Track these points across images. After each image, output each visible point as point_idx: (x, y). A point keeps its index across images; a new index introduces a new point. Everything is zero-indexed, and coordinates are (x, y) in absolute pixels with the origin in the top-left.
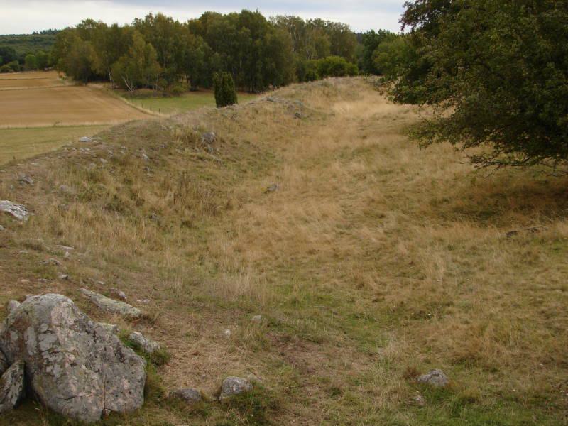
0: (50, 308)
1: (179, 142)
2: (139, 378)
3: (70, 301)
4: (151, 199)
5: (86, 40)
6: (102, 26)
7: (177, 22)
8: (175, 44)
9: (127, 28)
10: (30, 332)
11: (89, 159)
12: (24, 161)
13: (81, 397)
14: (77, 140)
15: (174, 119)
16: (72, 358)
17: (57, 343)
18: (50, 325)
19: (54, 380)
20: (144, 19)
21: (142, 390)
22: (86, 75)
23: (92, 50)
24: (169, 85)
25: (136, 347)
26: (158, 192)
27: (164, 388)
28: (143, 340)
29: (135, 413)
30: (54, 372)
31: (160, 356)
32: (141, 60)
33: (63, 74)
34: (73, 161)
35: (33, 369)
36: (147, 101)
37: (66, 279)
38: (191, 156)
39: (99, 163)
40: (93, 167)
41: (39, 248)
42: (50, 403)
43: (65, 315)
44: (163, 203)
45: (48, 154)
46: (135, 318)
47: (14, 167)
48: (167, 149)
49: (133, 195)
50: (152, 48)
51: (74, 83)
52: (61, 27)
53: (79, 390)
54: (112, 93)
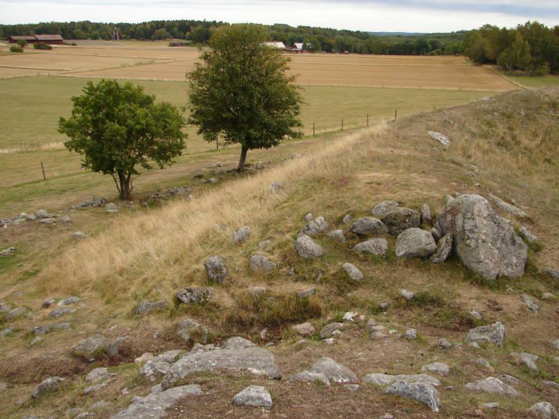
0: (474, 204)
1: (546, 106)
2: (523, 257)
3: (486, 201)
4: (525, 142)
5: (485, 37)
6: (496, 29)
7: (504, 29)
8: (543, 42)
9: (512, 30)
10: (459, 217)
11: (487, 112)
12: (448, 109)
13: (486, 263)
14: (480, 99)
15: (543, 90)
16: (484, 237)
17: (476, 226)
18: (473, 214)
20: (524, 25)
21: (524, 265)
22: (482, 59)
23: (488, 43)
24: (535, 69)
25: (523, 236)
26: (530, 138)
27: (538, 267)
28: (527, 233)
29: (517, 279)
31: (537, 245)
32: (519, 52)
33: (468, 58)
34: (478, 112)
35: (458, 238)
36: (519, 78)
37: (479, 186)
39: (493, 115)
40: (489, 117)
41: (459, 164)
42: (465, 263)
43: (482, 210)
44: (533, 145)
45: (462, 107)
46: (522, 218)
47: (441, 113)
48: (538, 110)
49: (514, 138)
50: (527, 44)
52: (469, 29)
53: (485, 259)
54: (497, 71)
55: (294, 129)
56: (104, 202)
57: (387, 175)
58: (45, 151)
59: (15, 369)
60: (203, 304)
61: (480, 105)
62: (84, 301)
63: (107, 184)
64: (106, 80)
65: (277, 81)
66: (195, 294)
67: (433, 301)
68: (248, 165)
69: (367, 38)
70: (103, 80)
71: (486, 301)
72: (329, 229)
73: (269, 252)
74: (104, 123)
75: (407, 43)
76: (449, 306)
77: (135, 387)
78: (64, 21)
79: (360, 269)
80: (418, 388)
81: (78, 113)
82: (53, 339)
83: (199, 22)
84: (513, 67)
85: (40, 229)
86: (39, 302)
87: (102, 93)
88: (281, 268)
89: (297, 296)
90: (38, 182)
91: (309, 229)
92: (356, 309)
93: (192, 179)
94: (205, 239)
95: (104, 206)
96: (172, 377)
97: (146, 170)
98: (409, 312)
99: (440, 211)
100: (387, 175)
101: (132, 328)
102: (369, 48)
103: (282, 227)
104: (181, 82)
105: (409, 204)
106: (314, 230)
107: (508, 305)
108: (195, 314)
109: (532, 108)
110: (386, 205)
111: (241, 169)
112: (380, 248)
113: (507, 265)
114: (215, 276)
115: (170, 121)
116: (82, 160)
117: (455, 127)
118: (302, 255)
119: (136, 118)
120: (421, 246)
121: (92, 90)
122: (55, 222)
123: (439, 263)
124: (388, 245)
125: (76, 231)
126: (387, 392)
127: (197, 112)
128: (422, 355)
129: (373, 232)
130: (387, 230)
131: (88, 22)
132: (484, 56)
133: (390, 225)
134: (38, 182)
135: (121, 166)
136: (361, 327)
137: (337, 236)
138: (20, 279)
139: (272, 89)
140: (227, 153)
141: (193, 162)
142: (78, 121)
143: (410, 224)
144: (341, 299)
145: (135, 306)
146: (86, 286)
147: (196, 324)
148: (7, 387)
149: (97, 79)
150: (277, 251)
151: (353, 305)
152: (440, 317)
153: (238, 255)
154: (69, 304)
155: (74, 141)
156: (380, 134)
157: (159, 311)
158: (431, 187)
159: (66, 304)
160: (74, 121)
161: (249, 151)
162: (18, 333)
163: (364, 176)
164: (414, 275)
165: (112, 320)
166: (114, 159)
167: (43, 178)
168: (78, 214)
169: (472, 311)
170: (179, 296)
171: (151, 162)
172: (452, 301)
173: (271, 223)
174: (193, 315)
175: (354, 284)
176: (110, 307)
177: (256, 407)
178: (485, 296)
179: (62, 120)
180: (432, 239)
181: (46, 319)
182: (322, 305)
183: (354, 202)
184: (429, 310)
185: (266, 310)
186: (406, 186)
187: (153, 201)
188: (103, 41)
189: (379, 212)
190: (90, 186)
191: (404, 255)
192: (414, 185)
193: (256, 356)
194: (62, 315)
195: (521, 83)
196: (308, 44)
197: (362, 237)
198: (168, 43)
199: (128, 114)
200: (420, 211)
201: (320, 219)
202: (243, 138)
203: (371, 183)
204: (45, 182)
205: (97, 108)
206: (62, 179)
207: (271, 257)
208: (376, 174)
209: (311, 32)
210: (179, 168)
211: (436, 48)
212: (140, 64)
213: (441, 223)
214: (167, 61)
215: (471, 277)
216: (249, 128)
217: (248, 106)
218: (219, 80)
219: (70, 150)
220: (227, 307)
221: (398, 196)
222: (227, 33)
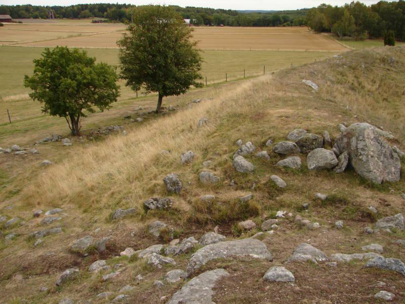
0: (364, 129)
1: (378, 61)
4: (368, 86)
5: (322, 13)
6: (329, 7)
7: (336, 7)
8: (363, 16)
10: (354, 140)
11: (338, 66)
12: (311, 64)
16: (372, 153)
17: (366, 146)
18: (364, 137)
19: (363, 162)
21: (399, 173)
22: (320, 29)
23: (324, 17)
28: (398, 150)
29: (396, 183)
30: (363, 159)
33: (310, 28)
34: (333, 66)
36: (348, 42)
38: (384, 68)
40: (341, 69)
42: (359, 172)
46: (391, 140)
48: (373, 64)
49: (360, 84)
51: (314, 32)
54: (332, 37)
55: (198, 81)
56: (60, 138)
57: (291, 111)
58: (7, 102)
59: (27, 264)
60: (167, 210)
61: (333, 60)
62: (66, 211)
63: (62, 124)
64: (60, 47)
65: (184, 46)
66: (160, 202)
67: (340, 201)
68: (163, 108)
69: (236, 15)
70: (58, 47)
71: (378, 199)
72: (256, 150)
73: (211, 169)
74: (59, 78)
75: (265, 18)
76: (353, 204)
77: (147, 273)
78: (11, 5)
79: (284, 180)
80: (393, 262)
81: (39, 72)
82: (51, 241)
83: (113, 5)
84: (343, 34)
85: (15, 159)
86: (28, 214)
87: (57, 57)
88: (224, 180)
89: (240, 201)
90: (5, 124)
91: (242, 151)
92: (284, 209)
93: (122, 119)
94: (156, 161)
95: (61, 141)
96: (196, 264)
97: (90, 113)
98: (324, 209)
99: (337, 136)
100: (290, 111)
101: (112, 230)
102: (238, 23)
103: (219, 151)
104: (103, 49)
105: (313, 131)
106: (245, 152)
107: (393, 202)
108: (161, 217)
109: (370, 62)
110: (298, 132)
111: (159, 111)
112: (296, 164)
113: (388, 173)
114: (172, 188)
115: (108, 76)
116: (42, 107)
117: (319, 77)
118: (239, 170)
119: (83, 74)
120: (328, 161)
121: (48, 54)
122: (26, 154)
123: (340, 173)
124: (301, 161)
125: (43, 160)
126: (368, 266)
127: (125, 70)
128: (355, 239)
129: (290, 152)
130: (300, 150)
131: (30, 5)
132: (322, 26)
133: (302, 146)
134: (5, 124)
135: (73, 110)
136: (291, 222)
137: (263, 156)
138: (7, 197)
139: (182, 51)
140: (147, 99)
141: (120, 107)
142: (38, 78)
143: (316, 145)
144: (271, 202)
145: (111, 214)
146: (64, 200)
147: (163, 225)
148: (23, 278)
149: (52, 47)
150: (219, 168)
151: (282, 206)
152: (347, 212)
153: (187, 172)
154: (55, 213)
155: (37, 93)
156: (269, 82)
157: (131, 216)
158: (325, 118)
159: (52, 214)
160: (37, 78)
161: (164, 98)
162: (20, 237)
163: (275, 112)
164: (323, 183)
165: (95, 224)
166: (68, 105)
167: (9, 121)
168: (43, 147)
169: (370, 207)
170: (146, 204)
171: (95, 108)
172: (354, 201)
173: (209, 148)
174: (160, 218)
175: (281, 191)
176: (89, 215)
177: (285, 282)
178: (376, 196)
179: (27, 77)
180: (334, 156)
181: (39, 226)
182: (259, 207)
183: (272, 131)
184: (337, 207)
185: (217, 212)
186: (307, 118)
187: (97, 136)
188: (42, 20)
189: (293, 138)
190: (46, 127)
191: (314, 168)
192: (313, 118)
193: (253, 244)
194: (51, 222)
195: (350, 46)
196: (194, 20)
197: (282, 156)
198: (91, 21)
199: (77, 72)
200: (323, 136)
201: (249, 144)
202: (161, 88)
203: (281, 116)
204: (11, 125)
205: (53, 67)
206: (24, 122)
207: (216, 173)
208: (283, 110)
209: (196, 11)
210: (115, 110)
211: (287, 22)
212: (71, 36)
213: (339, 144)
214: (91, 34)
215: (365, 183)
216: (165, 81)
217: (164, 65)
218: (142, 46)
219: (34, 100)
220: (187, 210)
221: (304, 126)
222: (146, 11)
